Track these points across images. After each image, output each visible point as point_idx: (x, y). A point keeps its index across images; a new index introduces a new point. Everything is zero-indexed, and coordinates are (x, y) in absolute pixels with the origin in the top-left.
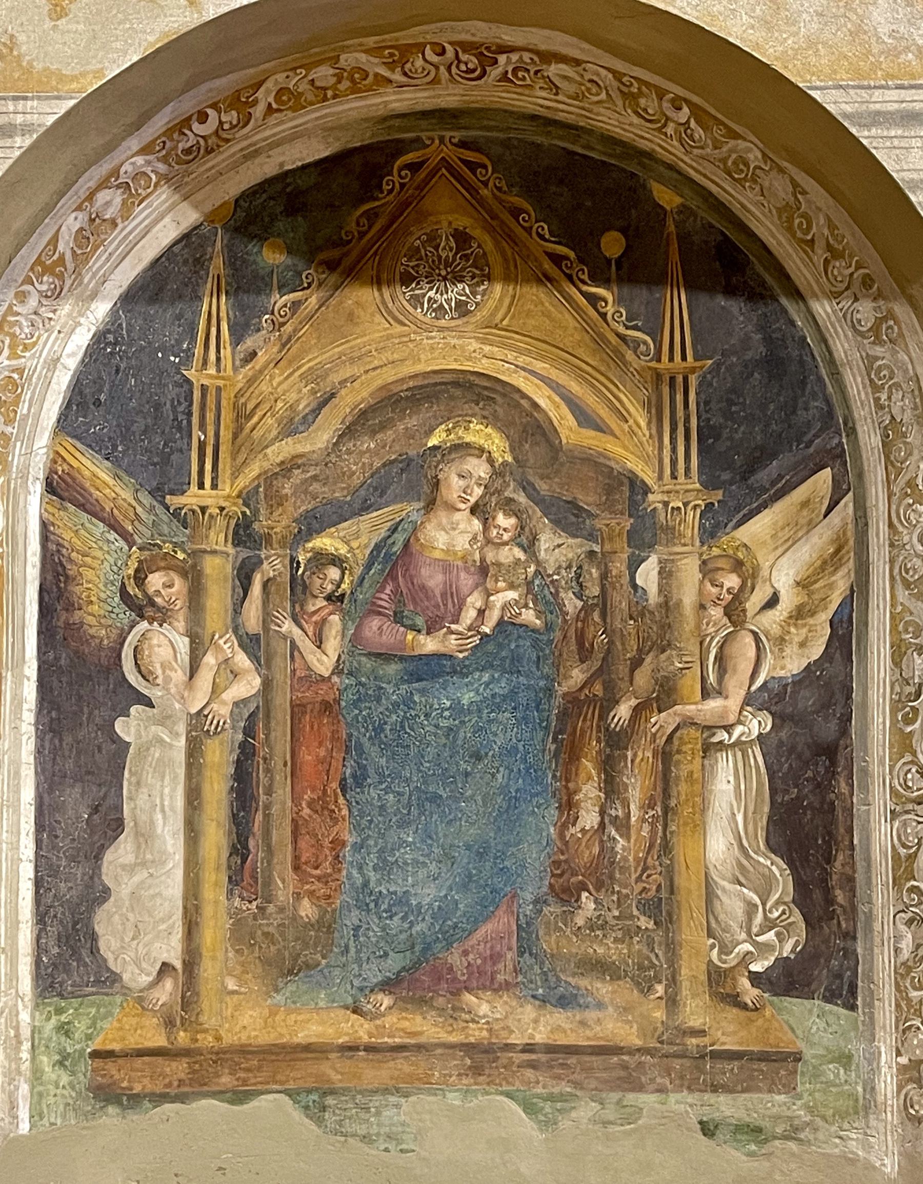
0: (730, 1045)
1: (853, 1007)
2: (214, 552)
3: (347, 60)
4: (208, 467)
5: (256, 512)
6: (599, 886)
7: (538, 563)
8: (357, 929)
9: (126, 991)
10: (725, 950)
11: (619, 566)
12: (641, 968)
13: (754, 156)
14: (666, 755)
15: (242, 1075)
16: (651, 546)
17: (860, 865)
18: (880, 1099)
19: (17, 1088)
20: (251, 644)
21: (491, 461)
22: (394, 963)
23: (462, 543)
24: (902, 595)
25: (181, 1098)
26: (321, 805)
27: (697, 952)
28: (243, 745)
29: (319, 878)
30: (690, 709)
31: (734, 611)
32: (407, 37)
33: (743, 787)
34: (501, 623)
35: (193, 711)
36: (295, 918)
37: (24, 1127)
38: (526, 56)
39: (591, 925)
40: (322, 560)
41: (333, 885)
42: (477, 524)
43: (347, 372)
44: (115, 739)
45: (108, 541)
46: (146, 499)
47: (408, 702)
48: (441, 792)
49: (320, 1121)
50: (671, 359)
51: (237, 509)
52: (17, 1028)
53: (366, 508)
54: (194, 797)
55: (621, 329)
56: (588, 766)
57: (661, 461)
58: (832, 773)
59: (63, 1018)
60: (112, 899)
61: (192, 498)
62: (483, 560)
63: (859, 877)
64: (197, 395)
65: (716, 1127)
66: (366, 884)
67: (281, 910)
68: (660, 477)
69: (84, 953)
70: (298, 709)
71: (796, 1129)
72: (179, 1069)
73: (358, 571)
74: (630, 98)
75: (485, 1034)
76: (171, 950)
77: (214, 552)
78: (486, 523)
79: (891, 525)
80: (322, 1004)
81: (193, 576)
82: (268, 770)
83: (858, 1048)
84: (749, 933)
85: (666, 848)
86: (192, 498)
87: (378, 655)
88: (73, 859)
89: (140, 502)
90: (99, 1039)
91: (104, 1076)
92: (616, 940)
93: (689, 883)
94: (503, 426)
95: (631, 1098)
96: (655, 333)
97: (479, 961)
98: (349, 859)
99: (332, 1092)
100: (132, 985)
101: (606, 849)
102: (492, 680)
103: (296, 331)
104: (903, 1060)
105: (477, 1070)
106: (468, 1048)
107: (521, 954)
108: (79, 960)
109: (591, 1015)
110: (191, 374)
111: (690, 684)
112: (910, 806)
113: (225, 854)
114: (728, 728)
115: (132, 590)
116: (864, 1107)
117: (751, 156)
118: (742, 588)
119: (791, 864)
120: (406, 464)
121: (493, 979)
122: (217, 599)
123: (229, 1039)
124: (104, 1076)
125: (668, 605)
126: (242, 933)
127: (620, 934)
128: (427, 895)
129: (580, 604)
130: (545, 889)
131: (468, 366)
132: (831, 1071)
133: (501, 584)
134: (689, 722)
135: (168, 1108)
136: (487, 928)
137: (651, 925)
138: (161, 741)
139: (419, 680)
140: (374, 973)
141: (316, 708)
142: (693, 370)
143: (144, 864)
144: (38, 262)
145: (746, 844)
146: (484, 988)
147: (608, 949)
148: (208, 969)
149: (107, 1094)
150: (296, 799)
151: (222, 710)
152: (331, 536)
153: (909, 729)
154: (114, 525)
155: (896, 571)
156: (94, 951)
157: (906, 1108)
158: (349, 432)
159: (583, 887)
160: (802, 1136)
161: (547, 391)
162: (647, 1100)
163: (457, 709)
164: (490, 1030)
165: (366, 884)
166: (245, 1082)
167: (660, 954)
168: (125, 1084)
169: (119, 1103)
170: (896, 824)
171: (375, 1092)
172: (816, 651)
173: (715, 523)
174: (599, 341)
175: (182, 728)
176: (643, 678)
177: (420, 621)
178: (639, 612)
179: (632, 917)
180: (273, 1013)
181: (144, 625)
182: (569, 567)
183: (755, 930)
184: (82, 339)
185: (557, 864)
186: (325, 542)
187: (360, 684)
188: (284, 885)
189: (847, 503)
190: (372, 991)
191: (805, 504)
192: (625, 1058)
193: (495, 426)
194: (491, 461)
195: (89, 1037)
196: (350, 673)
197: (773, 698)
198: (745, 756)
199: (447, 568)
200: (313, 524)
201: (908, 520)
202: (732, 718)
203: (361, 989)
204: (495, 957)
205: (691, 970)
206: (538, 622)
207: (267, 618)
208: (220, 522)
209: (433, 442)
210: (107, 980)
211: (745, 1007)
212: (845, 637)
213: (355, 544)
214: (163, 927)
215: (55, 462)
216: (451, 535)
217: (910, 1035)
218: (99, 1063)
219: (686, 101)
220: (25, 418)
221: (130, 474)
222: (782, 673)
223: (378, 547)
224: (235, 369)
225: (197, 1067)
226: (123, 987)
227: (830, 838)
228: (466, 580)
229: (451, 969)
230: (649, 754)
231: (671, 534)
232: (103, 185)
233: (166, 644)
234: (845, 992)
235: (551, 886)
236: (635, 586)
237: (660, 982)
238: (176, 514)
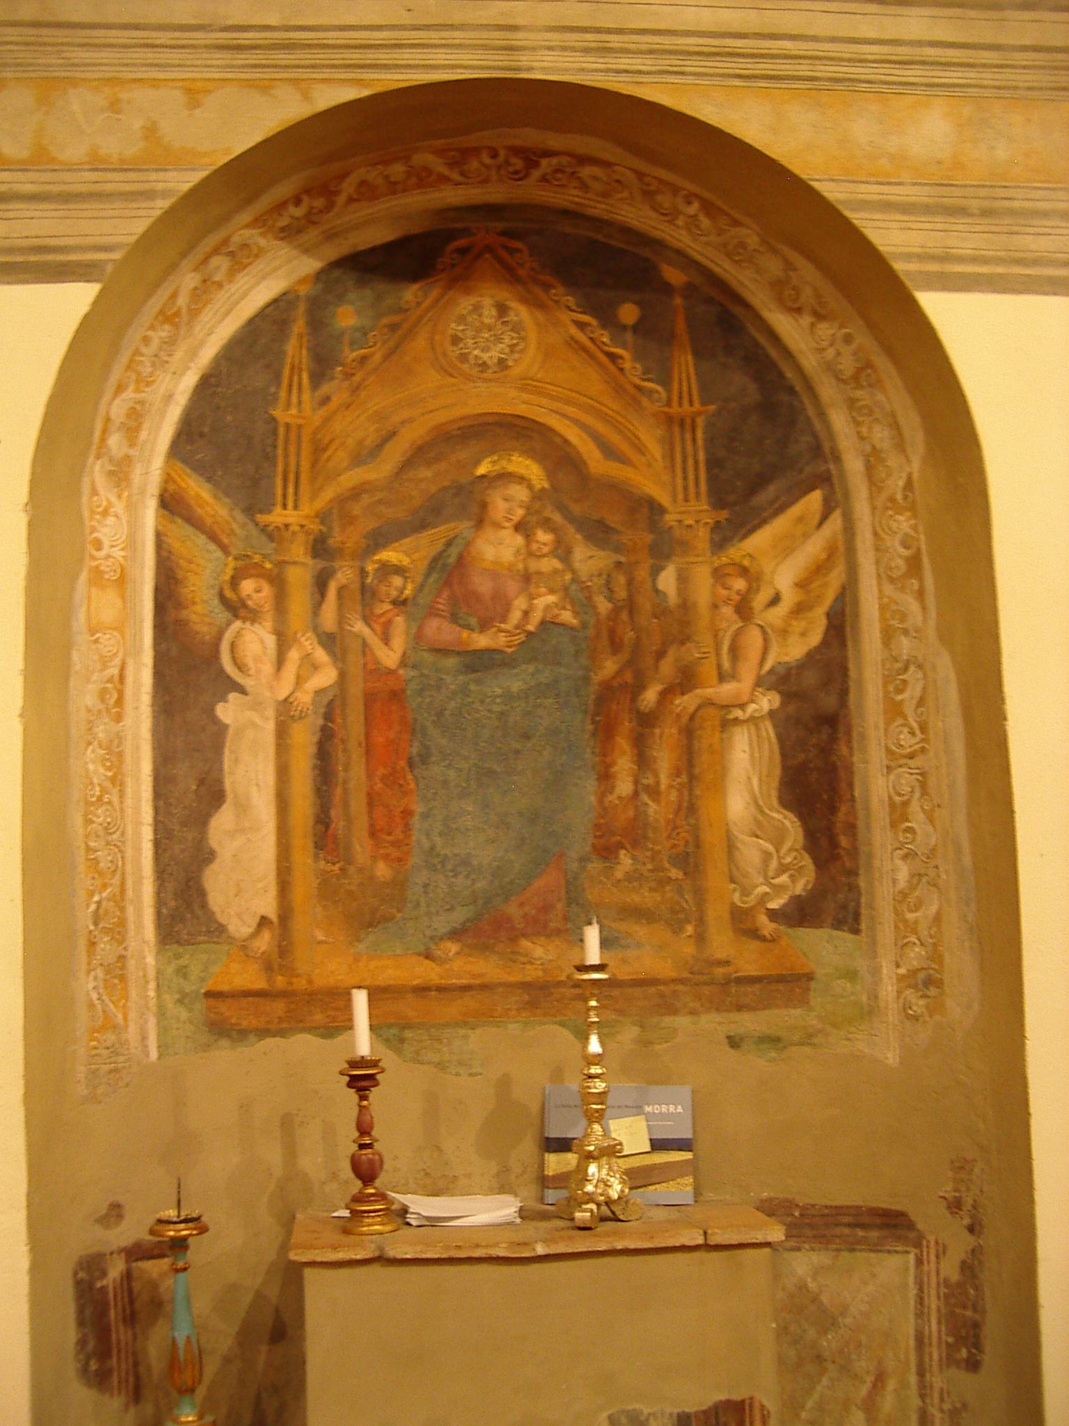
0: (751, 970)
1: (856, 931)
2: (295, 563)
3: (420, 159)
4: (291, 490)
5: (330, 528)
6: (635, 843)
7: (573, 571)
8: (426, 886)
9: (231, 940)
10: (745, 892)
11: (642, 573)
12: (674, 912)
13: (753, 241)
14: (689, 732)
15: (333, 1013)
16: (668, 557)
17: (861, 813)
18: (882, 1004)
19: (146, 1022)
20: (329, 641)
21: (530, 487)
22: (460, 916)
23: (507, 555)
24: (888, 589)
25: (281, 1033)
26: (392, 779)
27: (721, 896)
28: (324, 729)
29: (393, 844)
30: (709, 692)
31: (743, 609)
32: (471, 140)
33: (757, 755)
34: (543, 623)
35: (281, 697)
36: (372, 878)
37: (154, 1054)
38: (565, 160)
39: (629, 877)
40: (388, 570)
41: (405, 848)
42: (519, 540)
43: (406, 414)
44: (215, 720)
45: (208, 551)
46: (240, 517)
47: (465, 691)
48: (495, 767)
49: (399, 1052)
50: (680, 405)
51: (315, 527)
52: (144, 970)
53: (422, 526)
54: (283, 772)
55: (637, 381)
56: (623, 743)
57: (674, 488)
58: (833, 739)
59: (182, 962)
60: (218, 860)
61: (277, 517)
62: (526, 569)
63: (861, 824)
64: (281, 430)
65: (741, 1039)
66: (432, 848)
67: (361, 870)
68: (675, 501)
69: (196, 907)
70: (370, 699)
71: (811, 1036)
72: (279, 1007)
73: (419, 579)
74: (648, 195)
75: (540, 973)
76: (267, 905)
77: (295, 563)
78: (529, 537)
79: (876, 534)
80: (398, 952)
81: (278, 582)
82: (345, 750)
83: (861, 964)
84: (766, 878)
85: (692, 809)
86: (277, 517)
87: (438, 651)
88: (184, 824)
89: (234, 519)
90: (210, 982)
91: (216, 1013)
92: (651, 889)
93: (712, 837)
94: (540, 458)
95: (667, 1021)
96: (666, 382)
97: (534, 912)
98: (417, 826)
99: (409, 1026)
100: (237, 935)
101: (640, 815)
102: (538, 671)
103: (364, 380)
104: (902, 971)
105: (532, 1005)
106: (526, 986)
107: (569, 905)
108: (192, 912)
109: (631, 953)
110: (278, 413)
111: (708, 670)
112: (903, 761)
113: (311, 822)
114: (742, 706)
115: (229, 594)
116: (869, 1011)
117: (749, 241)
118: (749, 591)
119: (801, 816)
120: (458, 489)
121: (545, 927)
122: (299, 601)
123: (320, 982)
124: (216, 1013)
125: (686, 606)
126: (327, 890)
127: (653, 885)
128: (485, 856)
129: (610, 605)
130: (588, 849)
131: (508, 410)
132: (841, 985)
133: (543, 590)
134: (709, 703)
135: (270, 1042)
136: (539, 883)
137: (680, 875)
138: (254, 725)
139: (474, 671)
140: (443, 924)
141: (385, 698)
142: (699, 414)
143: (242, 831)
144: (161, 312)
145: (761, 803)
146: (538, 934)
147: (645, 897)
148: (300, 923)
149: (221, 1029)
150: (370, 775)
151: (305, 698)
152: (395, 550)
153: (899, 697)
154: (213, 538)
155: (882, 570)
156: (204, 905)
157: (904, 1009)
158: (407, 464)
159: (620, 846)
160: (815, 1041)
161: (576, 430)
162: (682, 1021)
163: (508, 697)
164: (544, 970)
165: (432, 848)
166: (334, 1019)
167: (690, 901)
168: (233, 1021)
169: (229, 1036)
170: (892, 777)
171: (447, 1025)
172: (815, 638)
173: (723, 536)
174: (619, 390)
175: (271, 713)
176: (667, 667)
177: (473, 621)
178: (661, 612)
179: (663, 870)
180: (357, 959)
181: (238, 624)
182: (600, 575)
183: (771, 874)
184: (190, 380)
185: (597, 826)
186: (390, 555)
187: (422, 675)
188: (361, 849)
189: (836, 521)
190: (442, 939)
191: (800, 519)
192: (661, 988)
193: (533, 458)
194: (530, 487)
195: (203, 980)
196: (414, 667)
197: (783, 681)
198: (758, 729)
199: (495, 575)
200: (378, 540)
201: (890, 529)
202: (745, 698)
203: (432, 938)
204: (546, 908)
205: (716, 913)
206: (575, 621)
207: (341, 620)
208: (301, 538)
209: (482, 470)
210: (217, 931)
211: (763, 939)
212: (840, 626)
213: (415, 556)
214: (260, 885)
215: (166, 482)
216: (498, 548)
217: (907, 950)
218: (212, 1001)
219: (696, 196)
220: (145, 442)
221: (227, 495)
222: (787, 659)
223: (435, 560)
224: (314, 410)
225: (293, 1006)
226: (229, 937)
227: (834, 790)
228: (512, 587)
229: (509, 919)
230: (674, 731)
231: (685, 546)
232: (216, 251)
233: (256, 641)
234: (850, 919)
235: (594, 846)
236: (657, 591)
237: (690, 922)
238: (264, 529)
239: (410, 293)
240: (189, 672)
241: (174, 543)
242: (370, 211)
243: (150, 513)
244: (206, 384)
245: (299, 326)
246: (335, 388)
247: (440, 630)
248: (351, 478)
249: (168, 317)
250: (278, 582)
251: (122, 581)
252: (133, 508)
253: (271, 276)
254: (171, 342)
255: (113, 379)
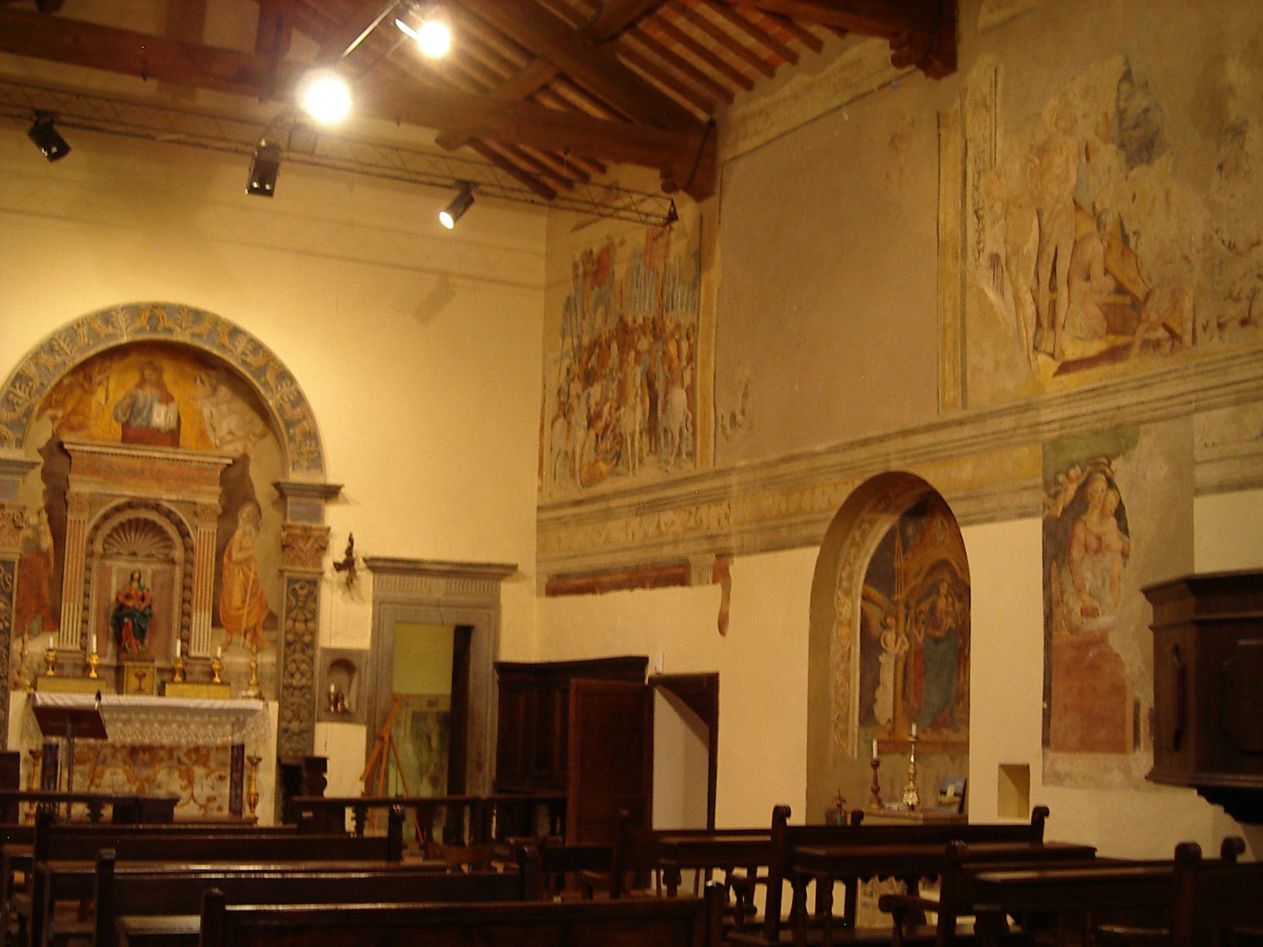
20: (908, 636)
76: (890, 715)
81: (897, 618)
151: (902, 654)
158: (925, 578)
184: (867, 560)
200: (919, 602)
233: (890, 636)
239: (924, 521)
240: (871, 647)
241: (866, 609)
242: (1097, 407)
243: (859, 603)
244: (873, 561)
245: (898, 536)
246: (909, 555)
247: (930, 631)
248: (912, 584)
249: (854, 544)
250: (897, 618)
251: (850, 623)
252: (853, 602)
253: (884, 525)
254: (859, 551)
255: (840, 566)
